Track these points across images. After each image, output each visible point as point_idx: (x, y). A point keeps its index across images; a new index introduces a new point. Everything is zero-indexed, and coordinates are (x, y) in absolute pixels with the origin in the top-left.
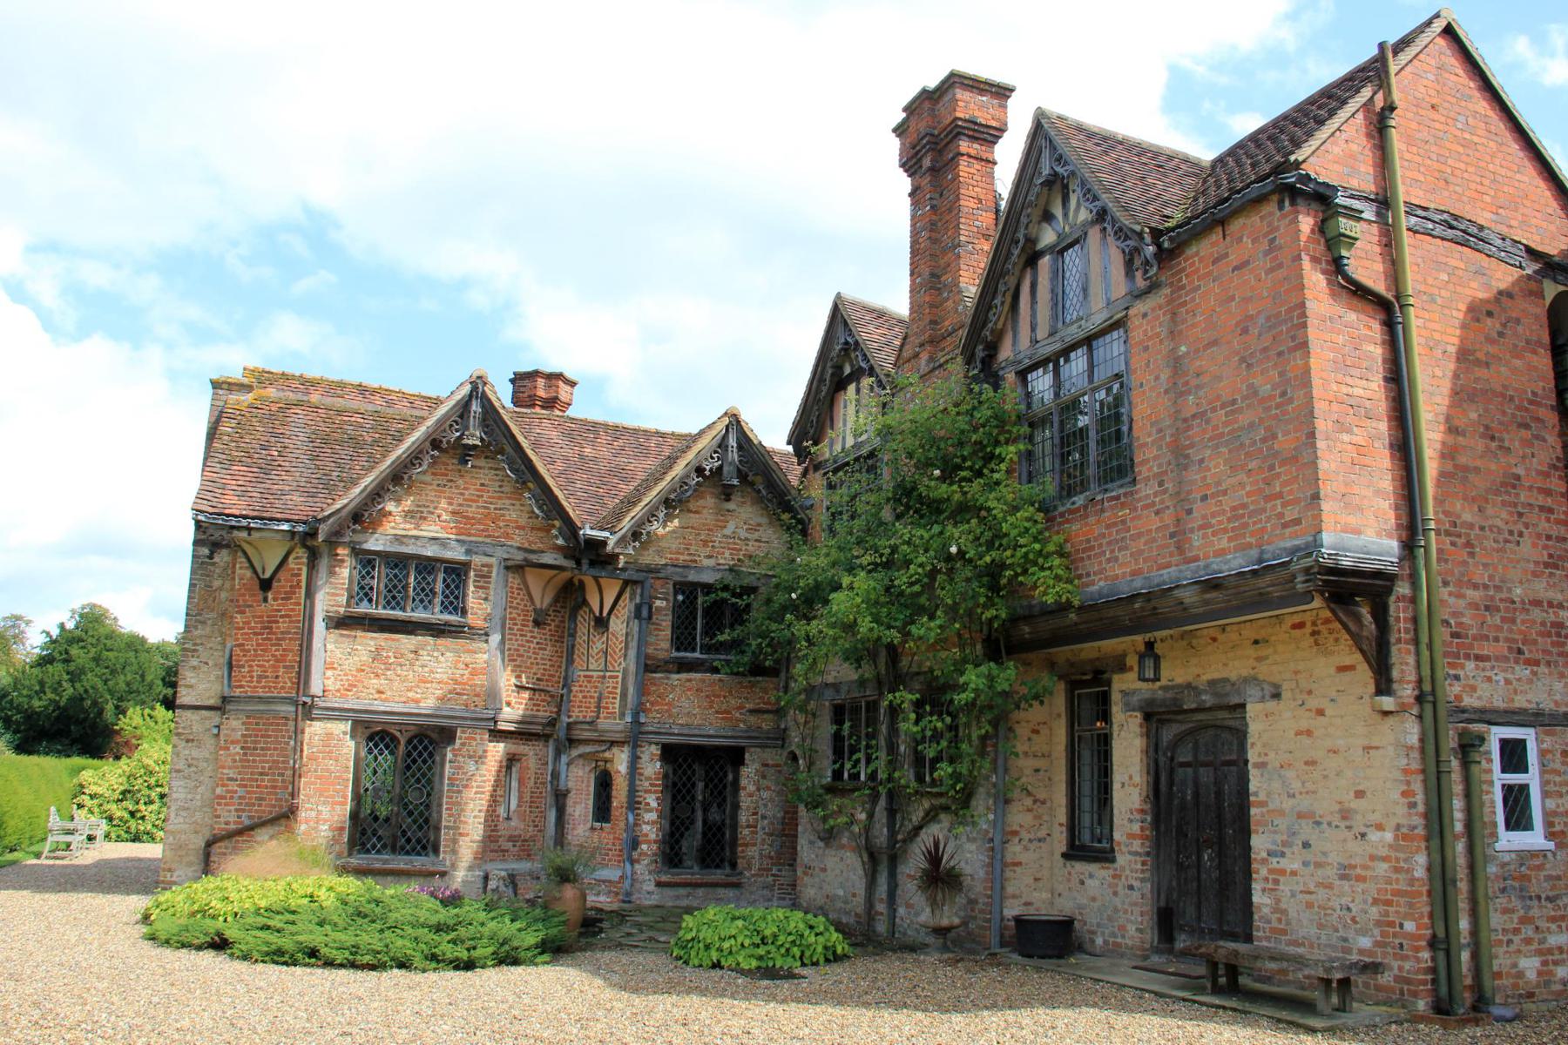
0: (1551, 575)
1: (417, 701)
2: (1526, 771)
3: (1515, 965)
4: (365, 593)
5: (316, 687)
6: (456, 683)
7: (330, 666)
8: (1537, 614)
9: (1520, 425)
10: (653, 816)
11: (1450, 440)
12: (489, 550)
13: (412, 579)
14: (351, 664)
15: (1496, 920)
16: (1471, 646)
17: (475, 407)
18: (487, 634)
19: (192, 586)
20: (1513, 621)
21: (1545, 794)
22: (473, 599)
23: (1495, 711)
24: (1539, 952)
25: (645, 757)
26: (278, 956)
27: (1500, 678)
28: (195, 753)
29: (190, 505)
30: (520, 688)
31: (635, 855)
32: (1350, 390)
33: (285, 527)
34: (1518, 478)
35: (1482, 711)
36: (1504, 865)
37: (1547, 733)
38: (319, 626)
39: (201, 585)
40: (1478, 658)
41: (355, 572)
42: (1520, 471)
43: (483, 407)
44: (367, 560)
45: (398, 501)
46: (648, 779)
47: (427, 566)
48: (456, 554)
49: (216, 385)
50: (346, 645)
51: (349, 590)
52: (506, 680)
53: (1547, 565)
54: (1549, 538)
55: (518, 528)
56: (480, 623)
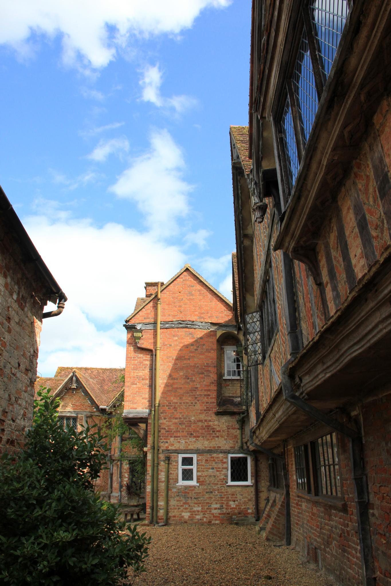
0: (207, 413)
2: (192, 465)
3: (181, 514)
8: (200, 424)
9: (200, 374)
10: (127, 479)
11: (171, 381)
15: (172, 502)
16: (173, 434)
17: (74, 378)
20: (190, 426)
21: (198, 471)
23: (182, 450)
24: (190, 512)
25: (124, 464)
27: (183, 441)
31: (122, 489)
34: (197, 388)
35: (176, 450)
36: (178, 489)
37: (200, 455)
40: (175, 437)
42: (198, 386)
53: (205, 410)
54: (207, 403)
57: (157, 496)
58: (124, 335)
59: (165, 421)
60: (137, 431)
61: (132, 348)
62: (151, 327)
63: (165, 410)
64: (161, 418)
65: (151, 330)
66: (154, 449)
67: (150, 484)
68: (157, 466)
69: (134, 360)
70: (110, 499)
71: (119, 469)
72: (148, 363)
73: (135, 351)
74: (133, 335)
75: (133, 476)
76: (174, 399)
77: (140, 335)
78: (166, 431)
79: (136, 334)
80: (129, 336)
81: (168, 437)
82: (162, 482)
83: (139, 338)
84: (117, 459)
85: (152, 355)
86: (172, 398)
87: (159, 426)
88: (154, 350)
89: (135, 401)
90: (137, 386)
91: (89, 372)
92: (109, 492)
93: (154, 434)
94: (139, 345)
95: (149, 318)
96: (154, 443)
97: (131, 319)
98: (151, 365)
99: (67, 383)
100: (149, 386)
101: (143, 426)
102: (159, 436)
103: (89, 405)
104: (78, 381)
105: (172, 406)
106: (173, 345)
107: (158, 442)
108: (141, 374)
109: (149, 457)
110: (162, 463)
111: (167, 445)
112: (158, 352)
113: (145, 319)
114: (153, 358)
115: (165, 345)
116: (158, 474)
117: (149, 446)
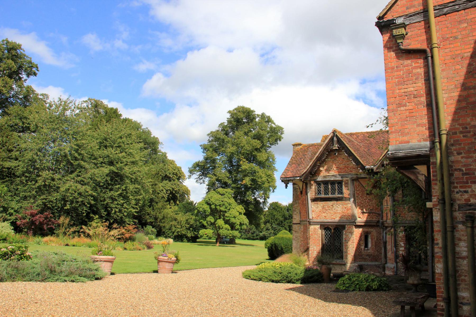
1: (334, 219)
4: (319, 192)
5: (311, 217)
6: (343, 213)
7: (313, 211)
10: (403, 249)
11: (465, 94)
12: (347, 176)
13: (330, 187)
14: (317, 210)
18: (350, 199)
19: (293, 194)
22: (344, 190)
26: (273, 281)
28: (297, 235)
29: (280, 176)
30: (363, 213)
31: (398, 260)
32: (406, 90)
33: (298, 178)
38: (310, 201)
39: (295, 194)
41: (316, 187)
43: (337, 138)
44: (318, 183)
45: (323, 167)
46: (400, 237)
47: (333, 183)
48: (339, 178)
49: (294, 145)
50: (316, 205)
51: (315, 191)
52: (357, 211)
55: (354, 168)
56: (347, 196)
57: (455, 281)
58: (378, 39)
59: (459, 158)
60: (412, 177)
61: (393, 54)
62: (420, 18)
63: (458, 140)
64: (452, 153)
65: (419, 22)
66: (444, 203)
67: (441, 260)
68: (452, 232)
69: (397, 71)
70: (384, 271)
71: (393, 237)
72: (421, 71)
73: (398, 57)
74: (392, 34)
75: (411, 245)
76: (472, 120)
77: (402, 31)
78: (463, 174)
79: (395, 32)
80: (387, 36)
81: (467, 183)
82: (464, 258)
83: (403, 37)
84: (391, 225)
85: (426, 58)
86: (469, 120)
87: (450, 167)
88: (428, 50)
89: (406, 131)
90: (407, 108)
91: (355, 137)
92: (383, 262)
93: (442, 179)
94: (402, 47)
95: (414, 6)
96: (443, 193)
97: (386, 14)
98: (427, 73)
99: (327, 145)
100: (428, 105)
101: (422, 169)
102: (451, 183)
103: (354, 167)
104: (339, 141)
105: (470, 132)
106: (460, 37)
107: (451, 192)
108: (412, 89)
109: (437, 216)
110: (460, 226)
111: (466, 196)
112: (436, 51)
113: (407, 8)
114: (427, 62)
115: (446, 40)
116: (454, 245)
117: (434, 199)
